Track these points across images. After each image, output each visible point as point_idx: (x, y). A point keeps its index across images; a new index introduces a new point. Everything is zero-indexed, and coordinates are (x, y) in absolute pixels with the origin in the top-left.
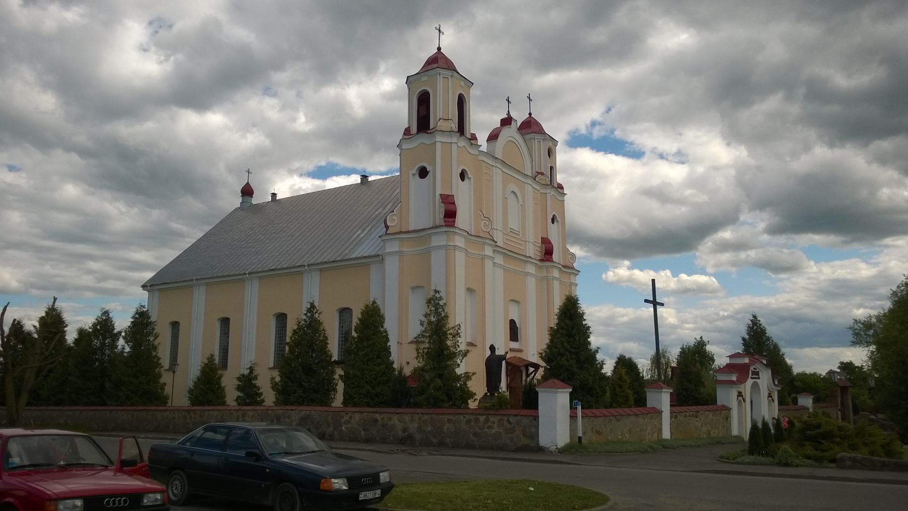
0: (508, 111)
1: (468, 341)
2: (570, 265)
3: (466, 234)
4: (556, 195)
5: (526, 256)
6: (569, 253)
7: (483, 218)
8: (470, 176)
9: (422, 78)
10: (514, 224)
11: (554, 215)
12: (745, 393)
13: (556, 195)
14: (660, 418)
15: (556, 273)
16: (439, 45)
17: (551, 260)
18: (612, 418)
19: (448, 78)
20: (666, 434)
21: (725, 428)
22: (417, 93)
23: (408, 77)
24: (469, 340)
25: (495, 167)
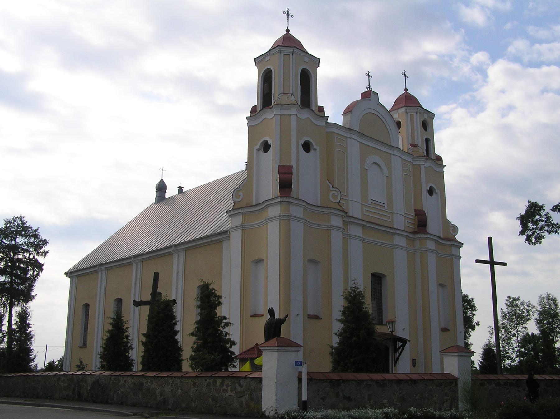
0: (369, 85)
1: (442, 327)
3: (304, 204)
4: (433, 167)
6: (450, 225)
7: (332, 189)
8: (437, 192)
9: (266, 58)
13: (433, 167)
15: (431, 245)
16: (288, 27)
17: (425, 232)
19: (289, 55)
24: (443, 326)
25: (393, 155)
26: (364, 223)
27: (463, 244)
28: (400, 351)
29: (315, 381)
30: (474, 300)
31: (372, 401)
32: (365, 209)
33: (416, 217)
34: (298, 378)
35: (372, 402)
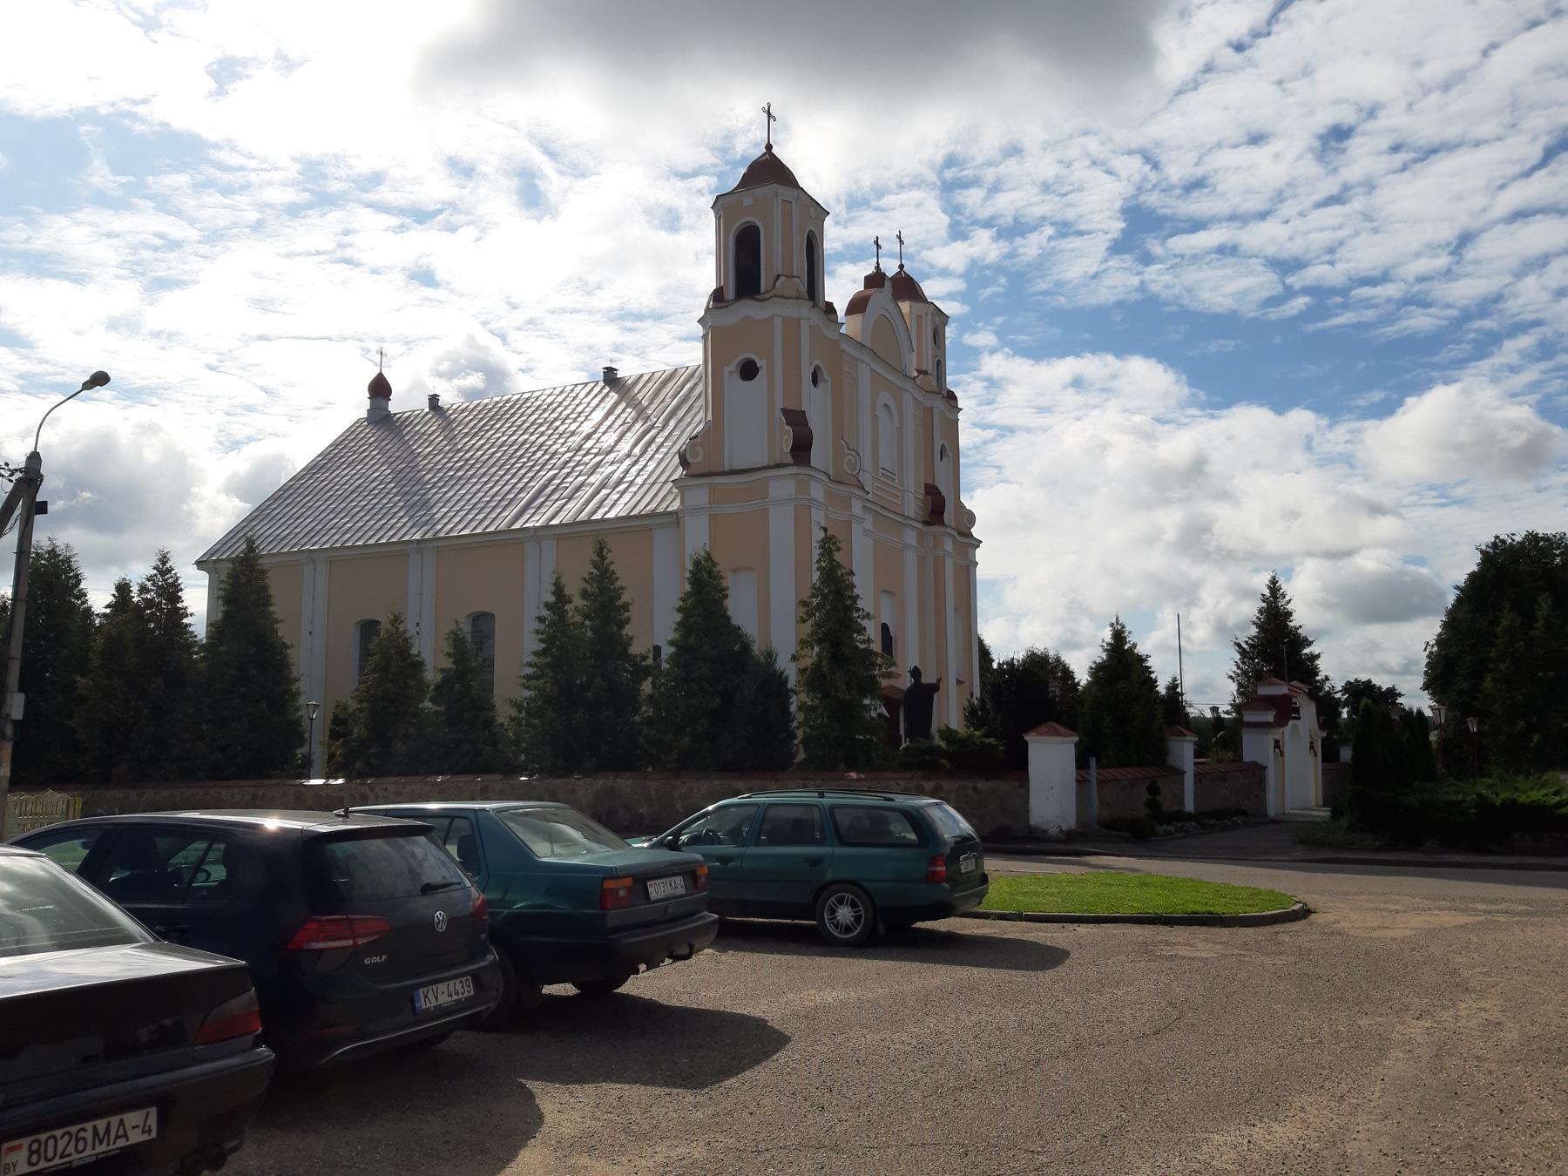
5: (903, 515)
7: (847, 451)
10: (886, 461)
11: (943, 445)
12: (1283, 743)
17: (942, 523)
19: (791, 202)
20: (1189, 806)
22: (738, 224)
23: (718, 197)
26: (878, 509)
27: (981, 542)
30: (1396, 687)
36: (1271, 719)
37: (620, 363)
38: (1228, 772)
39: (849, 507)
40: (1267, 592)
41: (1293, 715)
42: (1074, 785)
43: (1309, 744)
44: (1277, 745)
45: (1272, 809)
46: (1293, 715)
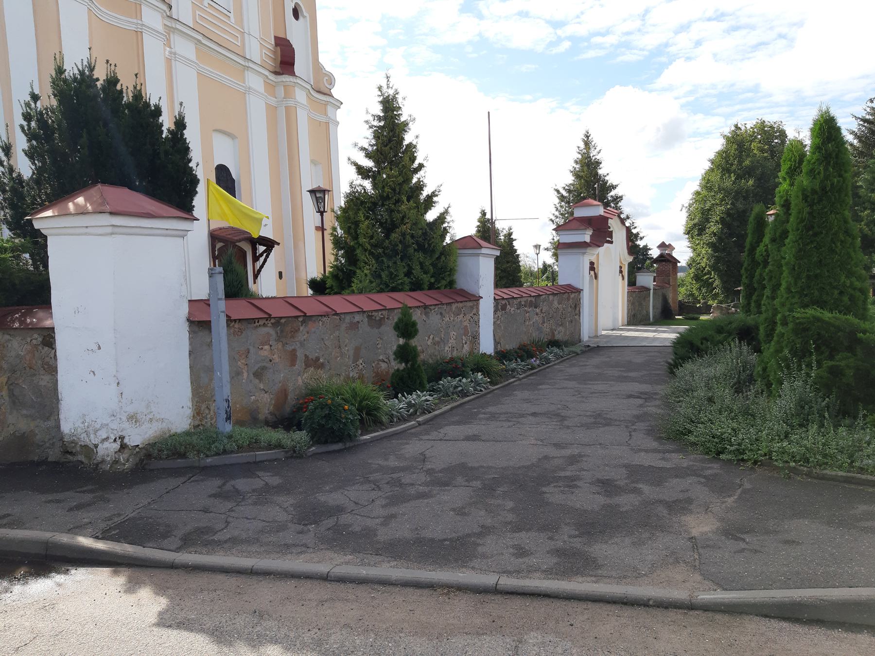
2: (326, 91)
6: (324, 72)
14: (475, 310)
17: (292, 73)
18: (358, 318)
21: (573, 324)
26: (200, 37)
28: (262, 259)
29: (237, 326)
31: (361, 361)
32: (198, 12)
33: (279, 48)
34: (188, 320)
35: (362, 364)
36: (587, 239)
37: (353, 158)
38: (540, 295)
39: (138, 14)
40: (582, 146)
41: (608, 239)
42: (185, 328)
43: (619, 269)
44: (592, 267)
45: (586, 334)
46: (608, 239)
